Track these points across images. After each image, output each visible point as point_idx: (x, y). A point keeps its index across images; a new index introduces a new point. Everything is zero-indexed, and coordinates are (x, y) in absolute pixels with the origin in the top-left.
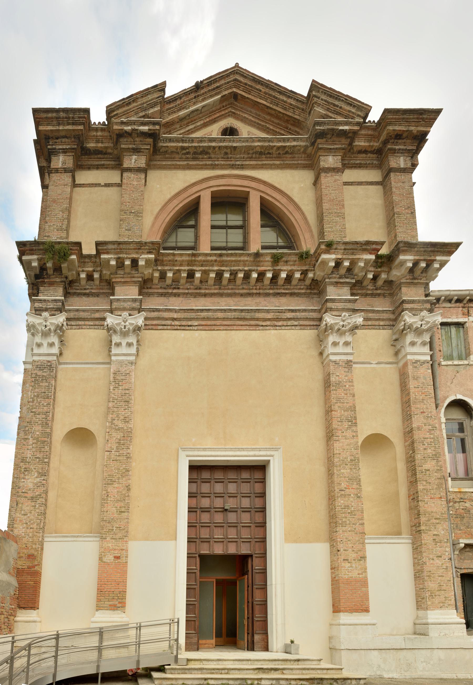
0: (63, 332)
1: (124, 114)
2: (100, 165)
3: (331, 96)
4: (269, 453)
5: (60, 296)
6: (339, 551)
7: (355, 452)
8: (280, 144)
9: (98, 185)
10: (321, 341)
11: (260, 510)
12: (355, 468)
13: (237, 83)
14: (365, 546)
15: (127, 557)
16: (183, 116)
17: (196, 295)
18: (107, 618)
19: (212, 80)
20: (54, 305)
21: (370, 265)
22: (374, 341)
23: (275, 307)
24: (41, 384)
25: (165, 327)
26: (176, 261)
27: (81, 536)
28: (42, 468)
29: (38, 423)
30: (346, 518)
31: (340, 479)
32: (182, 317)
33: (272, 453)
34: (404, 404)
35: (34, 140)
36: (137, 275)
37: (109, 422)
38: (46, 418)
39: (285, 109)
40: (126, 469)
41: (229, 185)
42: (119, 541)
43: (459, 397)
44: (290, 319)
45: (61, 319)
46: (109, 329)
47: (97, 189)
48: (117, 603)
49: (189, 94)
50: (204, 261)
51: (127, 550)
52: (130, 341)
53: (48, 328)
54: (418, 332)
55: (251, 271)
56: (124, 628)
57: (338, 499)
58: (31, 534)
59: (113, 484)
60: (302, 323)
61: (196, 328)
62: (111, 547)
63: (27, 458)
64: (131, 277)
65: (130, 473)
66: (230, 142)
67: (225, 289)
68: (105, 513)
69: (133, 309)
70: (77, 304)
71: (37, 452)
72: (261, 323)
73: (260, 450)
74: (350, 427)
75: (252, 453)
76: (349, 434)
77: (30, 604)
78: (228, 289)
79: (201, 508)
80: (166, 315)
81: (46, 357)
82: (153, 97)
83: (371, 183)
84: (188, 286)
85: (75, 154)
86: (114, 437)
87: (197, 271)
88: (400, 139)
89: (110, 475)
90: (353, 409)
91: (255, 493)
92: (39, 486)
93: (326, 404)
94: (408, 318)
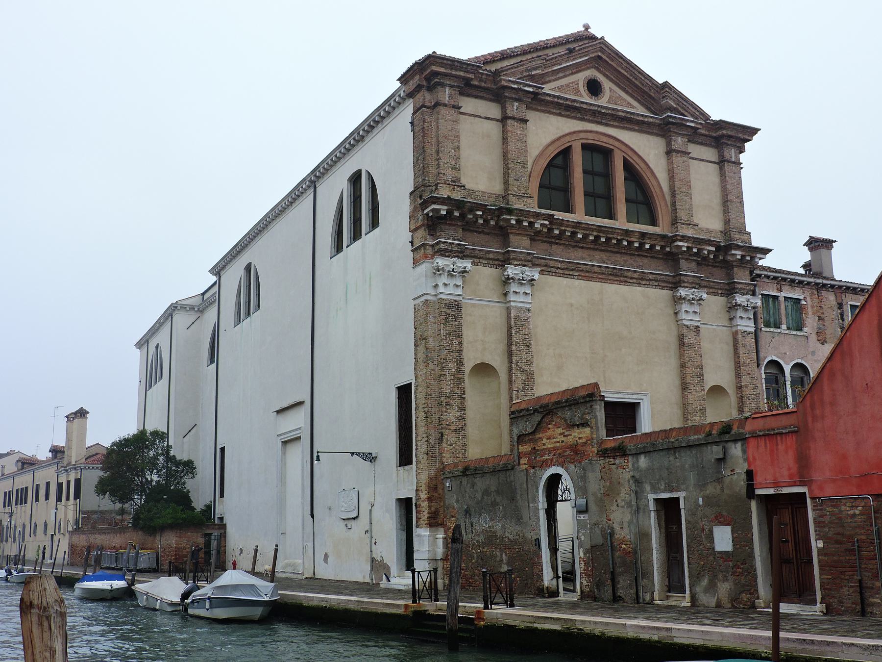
4: (639, 397)
9: (480, 117)
13: (602, 50)
22: (715, 303)
33: (642, 397)
43: (774, 358)
54: (745, 309)
72: (629, 280)
75: (627, 396)
76: (698, 388)
83: (711, 162)
90: (701, 367)
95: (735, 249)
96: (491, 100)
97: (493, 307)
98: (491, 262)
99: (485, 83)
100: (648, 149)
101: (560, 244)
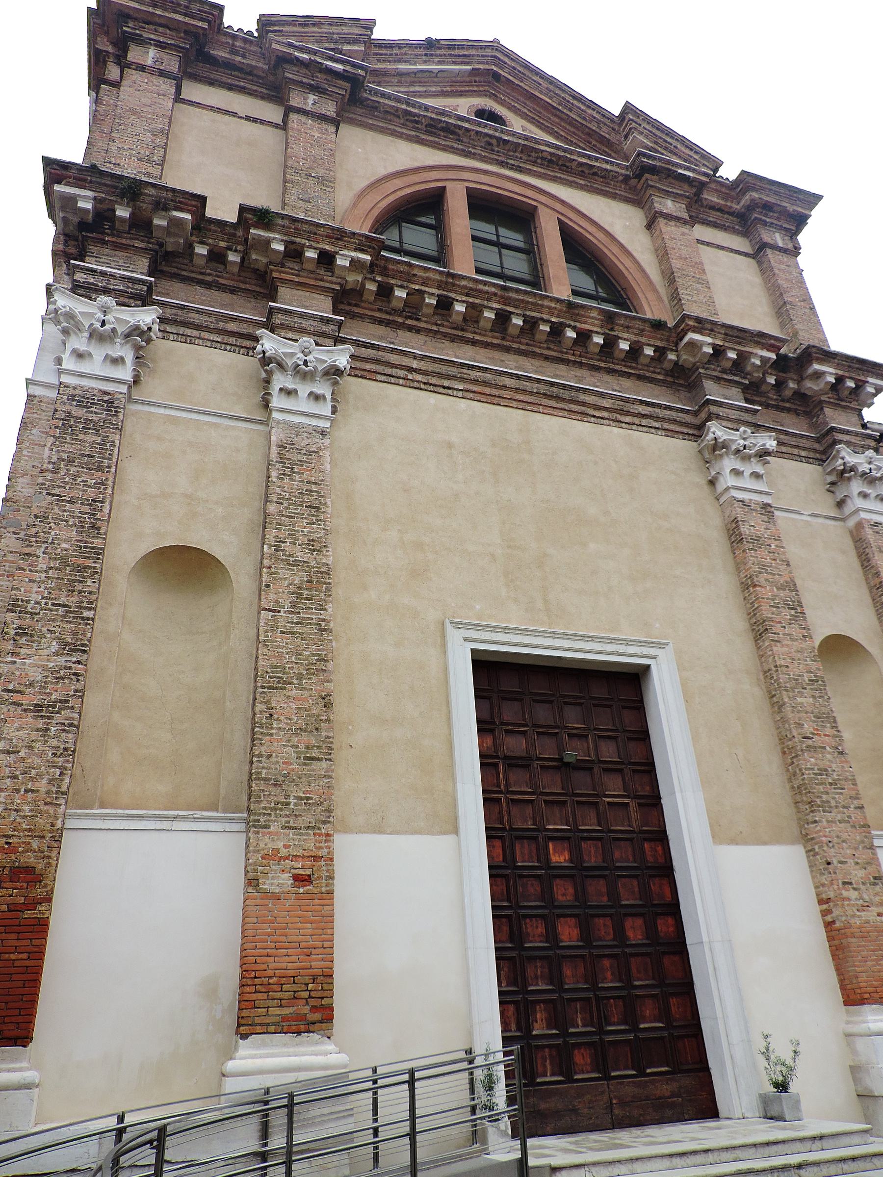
0: (149, 341)
1: (294, 35)
2: (237, 86)
3: (658, 129)
4: (646, 651)
5: (142, 273)
6: (829, 864)
7: (814, 666)
8: (584, 160)
9: (234, 114)
10: (707, 462)
11: (642, 768)
12: (820, 697)
14: (875, 854)
15: (331, 877)
16: (405, 71)
17: (453, 339)
18: (272, 1061)
19: (452, 45)
20: (129, 287)
21: (769, 365)
23: (613, 390)
24: (81, 437)
25: (393, 380)
26: (415, 275)
27: (184, 818)
28: (75, 633)
29: (66, 521)
30: (827, 793)
31: (798, 715)
32: (431, 369)
34: (874, 591)
35: (89, 9)
36: (330, 278)
37: (269, 545)
38: (94, 515)
39: (584, 119)
40: (320, 655)
41: (497, 187)
42: (307, 834)
44: (644, 416)
45: (147, 316)
46: (265, 361)
47: (227, 118)
48: (306, 1009)
49: (416, 48)
50: (471, 289)
51: (332, 859)
52: (319, 392)
53: (107, 327)
55: (563, 326)
56: (334, 1089)
57: (803, 754)
58: (27, 808)
59: (285, 689)
60: (666, 426)
61: (460, 394)
62: (284, 852)
63: (28, 601)
64: (316, 279)
65: (330, 665)
66: (489, 128)
67: (513, 342)
68: (263, 759)
69: (323, 335)
70: (178, 295)
71: (60, 590)
73: (627, 642)
74: (795, 618)
76: (794, 630)
77: (11, 1027)
78: (520, 343)
79: (506, 758)
80: (394, 358)
81: (101, 382)
82: (352, 31)
84: (438, 319)
85: (184, 56)
86: (285, 579)
87: (457, 301)
88: (769, 211)
89: (277, 667)
90: (792, 586)
91: (625, 731)
92: (63, 678)
93: (738, 570)
94: (716, 430)
95: (820, 361)
96: (263, 97)
97: (227, 428)
98: (232, 340)
99: (244, 57)
100: (615, 221)
101: (418, 331)
